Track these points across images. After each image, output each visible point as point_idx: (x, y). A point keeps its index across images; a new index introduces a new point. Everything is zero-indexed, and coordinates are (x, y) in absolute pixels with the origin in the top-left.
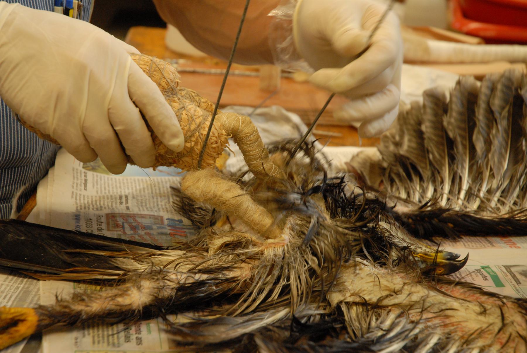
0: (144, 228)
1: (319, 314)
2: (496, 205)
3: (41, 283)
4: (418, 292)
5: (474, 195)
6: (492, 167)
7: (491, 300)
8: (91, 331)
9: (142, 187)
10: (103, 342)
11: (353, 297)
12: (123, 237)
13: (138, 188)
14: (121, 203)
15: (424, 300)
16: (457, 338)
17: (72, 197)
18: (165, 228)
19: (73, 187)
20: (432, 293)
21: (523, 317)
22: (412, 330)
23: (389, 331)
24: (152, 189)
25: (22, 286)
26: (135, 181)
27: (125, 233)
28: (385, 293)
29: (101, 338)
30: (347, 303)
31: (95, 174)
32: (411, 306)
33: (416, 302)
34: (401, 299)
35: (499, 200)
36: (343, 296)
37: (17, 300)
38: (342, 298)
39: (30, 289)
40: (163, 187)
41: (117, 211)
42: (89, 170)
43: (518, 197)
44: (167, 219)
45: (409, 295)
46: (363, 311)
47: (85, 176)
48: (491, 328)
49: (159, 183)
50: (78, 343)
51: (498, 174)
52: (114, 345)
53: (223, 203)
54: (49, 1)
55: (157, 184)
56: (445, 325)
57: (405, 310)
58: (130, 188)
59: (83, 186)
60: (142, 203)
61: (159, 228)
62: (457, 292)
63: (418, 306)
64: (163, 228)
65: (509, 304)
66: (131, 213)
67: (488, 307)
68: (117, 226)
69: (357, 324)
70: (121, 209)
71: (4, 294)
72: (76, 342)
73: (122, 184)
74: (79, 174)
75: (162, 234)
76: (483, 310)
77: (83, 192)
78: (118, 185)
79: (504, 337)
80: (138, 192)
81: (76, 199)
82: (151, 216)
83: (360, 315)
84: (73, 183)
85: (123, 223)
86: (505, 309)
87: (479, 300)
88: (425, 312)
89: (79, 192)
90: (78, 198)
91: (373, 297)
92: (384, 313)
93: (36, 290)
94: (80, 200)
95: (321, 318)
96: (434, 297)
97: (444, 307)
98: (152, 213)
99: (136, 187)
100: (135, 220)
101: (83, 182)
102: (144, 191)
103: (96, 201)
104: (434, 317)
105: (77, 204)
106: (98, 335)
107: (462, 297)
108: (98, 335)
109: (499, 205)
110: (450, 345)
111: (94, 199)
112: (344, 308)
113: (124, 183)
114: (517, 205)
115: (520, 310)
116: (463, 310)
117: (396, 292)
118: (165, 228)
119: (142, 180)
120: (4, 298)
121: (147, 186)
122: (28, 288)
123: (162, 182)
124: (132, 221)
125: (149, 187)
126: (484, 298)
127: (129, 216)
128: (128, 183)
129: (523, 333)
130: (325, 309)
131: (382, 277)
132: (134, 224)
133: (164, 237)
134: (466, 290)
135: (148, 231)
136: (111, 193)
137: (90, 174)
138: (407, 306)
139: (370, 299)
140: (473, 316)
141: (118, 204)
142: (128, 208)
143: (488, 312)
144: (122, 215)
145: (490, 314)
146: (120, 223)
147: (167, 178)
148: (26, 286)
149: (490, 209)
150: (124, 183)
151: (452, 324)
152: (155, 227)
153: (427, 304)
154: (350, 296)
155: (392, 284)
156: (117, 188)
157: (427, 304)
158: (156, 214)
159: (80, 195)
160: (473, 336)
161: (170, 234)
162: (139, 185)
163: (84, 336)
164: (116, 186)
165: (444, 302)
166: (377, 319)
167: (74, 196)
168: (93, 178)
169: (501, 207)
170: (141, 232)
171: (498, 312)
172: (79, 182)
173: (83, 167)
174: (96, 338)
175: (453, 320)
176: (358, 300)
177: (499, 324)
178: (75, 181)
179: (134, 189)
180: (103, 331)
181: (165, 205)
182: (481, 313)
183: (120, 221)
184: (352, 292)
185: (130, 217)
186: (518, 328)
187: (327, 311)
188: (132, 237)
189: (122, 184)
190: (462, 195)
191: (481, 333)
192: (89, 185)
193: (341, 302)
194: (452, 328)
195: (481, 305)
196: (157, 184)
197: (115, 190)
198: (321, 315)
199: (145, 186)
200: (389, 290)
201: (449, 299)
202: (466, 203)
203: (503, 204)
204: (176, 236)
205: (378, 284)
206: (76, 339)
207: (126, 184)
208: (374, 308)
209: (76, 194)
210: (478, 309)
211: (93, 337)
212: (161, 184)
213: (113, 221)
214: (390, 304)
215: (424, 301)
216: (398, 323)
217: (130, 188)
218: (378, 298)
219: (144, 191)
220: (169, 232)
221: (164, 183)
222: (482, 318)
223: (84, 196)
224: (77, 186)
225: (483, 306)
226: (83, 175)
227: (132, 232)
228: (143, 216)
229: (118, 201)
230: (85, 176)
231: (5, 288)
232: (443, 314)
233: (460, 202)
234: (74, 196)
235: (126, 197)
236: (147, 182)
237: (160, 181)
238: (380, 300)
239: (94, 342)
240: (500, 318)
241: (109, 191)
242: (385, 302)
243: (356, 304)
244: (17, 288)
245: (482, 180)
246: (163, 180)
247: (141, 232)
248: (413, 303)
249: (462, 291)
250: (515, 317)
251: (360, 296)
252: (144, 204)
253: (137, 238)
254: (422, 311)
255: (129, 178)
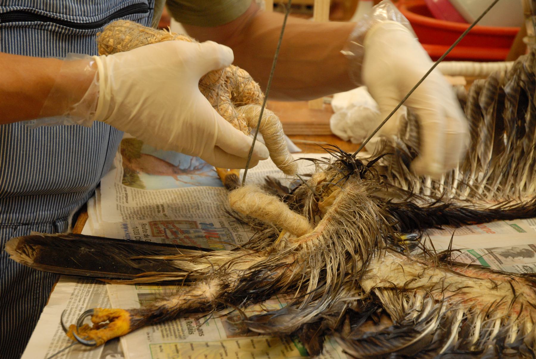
0: (183, 232)
1: (355, 300)
2: (483, 192)
3: (107, 286)
4: (437, 275)
5: (465, 184)
6: (480, 157)
7: (501, 277)
8: (159, 326)
9: (173, 197)
10: (171, 335)
11: (382, 283)
12: (167, 242)
13: (170, 198)
14: (159, 212)
15: (443, 280)
16: (478, 311)
17: (117, 209)
18: (201, 232)
19: (117, 200)
20: (449, 275)
21: (531, 288)
22: (440, 309)
23: (422, 311)
24: (182, 198)
25: (92, 289)
26: (166, 193)
27: (167, 238)
28: (409, 278)
29: (168, 332)
30: (380, 289)
31: (133, 188)
32: (432, 287)
33: (437, 283)
34: (424, 281)
35: (485, 187)
36: (375, 282)
37: (90, 302)
38: (373, 285)
39: (99, 292)
40: (191, 196)
41: (157, 219)
42: (127, 185)
43: (500, 183)
44: (200, 224)
45: (431, 277)
46: (394, 295)
47: (126, 191)
48: (504, 300)
49: (187, 193)
50: (150, 338)
51: (484, 164)
52: (180, 337)
53: (267, 214)
54: (25, 1)
55: (185, 193)
56: (465, 302)
57: (428, 291)
58: (164, 199)
59: (125, 199)
60: (176, 210)
61: (195, 232)
62: (470, 273)
63: (438, 286)
64: (199, 232)
65: (517, 279)
66: (169, 220)
67: (499, 283)
68: (160, 232)
69: (392, 306)
70: (160, 217)
71: (79, 297)
72: (149, 337)
73: (156, 196)
74: (120, 189)
75: (199, 237)
76: (494, 285)
77: (126, 205)
78: (153, 197)
79: (518, 307)
80: (171, 201)
81: (121, 211)
82: (187, 222)
83: (392, 299)
84: (117, 197)
85: (165, 229)
86: (513, 283)
87: (490, 278)
88: (445, 291)
89: (122, 205)
90: (122, 209)
91: (400, 282)
92: (411, 295)
93: (104, 292)
94: (124, 211)
95: (358, 304)
96: (451, 278)
97: (460, 286)
98: (187, 220)
99: (168, 197)
100: (174, 226)
101: (125, 195)
102: (176, 200)
103: (138, 211)
104: (454, 295)
105: (122, 215)
106: (166, 329)
107: (475, 276)
108: (166, 329)
109: (486, 192)
110: (476, 319)
111: (136, 210)
112: (378, 293)
113: (157, 195)
114: (500, 190)
115: (527, 283)
116: (478, 287)
117: (419, 276)
118: (201, 232)
119: (172, 191)
120: (79, 302)
121: (178, 196)
122: (97, 290)
123: (190, 192)
124: (172, 227)
125: (180, 196)
126: (494, 276)
127: (168, 222)
128: (161, 195)
129: (533, 302)
130: (359, 295)
131: (405, 264)
132: (174, 230)
133: (201, 239)
134: (477, 270)
135: (186, 235)
136: (149, 204)
137: (128, 188)
138: (429, 287)
139: (398, 284)
140: (487, 291)
141: (157, 212)
142: (165, 215)
143: (498, 287)
144: (162, 223)
145: (500, 288)
146: (163, 229)
147: (192, 188)
148: (95, 289)
149: (478, 196)
150: (157, 195)
151: (471, 300)
152: (192, 231)
153: (446, 285)
154: (380, 282)
155: (414, 270)
156: (152, 200)
157: (446, 285)
158: (190, 220)
159: (124, 207)
160: (491, 309)
161: (205, 237)
162: (171, 196)
163: (154, 331)
164: (152, 198)
165: (460, 281)
166: (408, 302)
167: (119, 208)
168: (132, 192)
169: (487, 194)
170: (181, 236)
171: (509, 286)
172: (121, 196)
173: (123, 183)
174: (164, 332)
175: (470, 296)
176: (387, 285)
177: (510, 297)
178: (118, 195)
179: (167, 199)
180: (169, 326)
181: (196, 211)
182: (493, 288)
183: (162, 227)
184: (381, 278)
185: (170, 223)
186: (528, 298)
187: (362, 297)
188: (174, 241)
189: (156, 196)
190: (455, 185)
191: (497, 305)
192: (130, 198)
193: (373, 289)
194: (472, 303)
195: (492, 281)
196: (185, 193)
197: (151, 200)
198: (358, 300)
199: (176, 196)
200: (413, 275)
201: (464, 279)
202: (459, 192)
203: (489, 190)
204: (211, 238)
205: (402, 271)
206: (148, 334)
207: (159, 196)
208: (401, 291)
209: (120, 206)
210: (490, 285)
211: (162, 331)
212: (189, 193)
213: (156, 228)
214: (416, 287)
215: (443, 281)
216: (427, 303)
217: (164, 199)
218: (404, 282)
219: (176, 200)
220: (204, 235)
221: (191, 192)
222: (494, 292)
223: (127, 208)
224: (120, 199)
225: (494, 282)
226: (123, 189)
227: (173, 237)
228: (180, 222)
229: (156, 210)
230: (126, 191)
231: (78, 293)
232: (461, 292)
233: (454, 191)
234: (119, 208)
235: (162, 206)
236: (176, 192)
237: (187, 190)
238: (406, 284)
239: (163, 336)
240: (511, 290)
241: (146, 202)
242: (411, 286)
243: (386, 289)
244: (88, 292)
245: (471, 171)
246: (190, 190)
247: (181, 236)
248: (434, 284)
249: (474, 271)
250: (525, 290)
251: (389, 282)
252: (178, 211)
253: (179, 242)
254: (443, 291)
255: (161, 191)
